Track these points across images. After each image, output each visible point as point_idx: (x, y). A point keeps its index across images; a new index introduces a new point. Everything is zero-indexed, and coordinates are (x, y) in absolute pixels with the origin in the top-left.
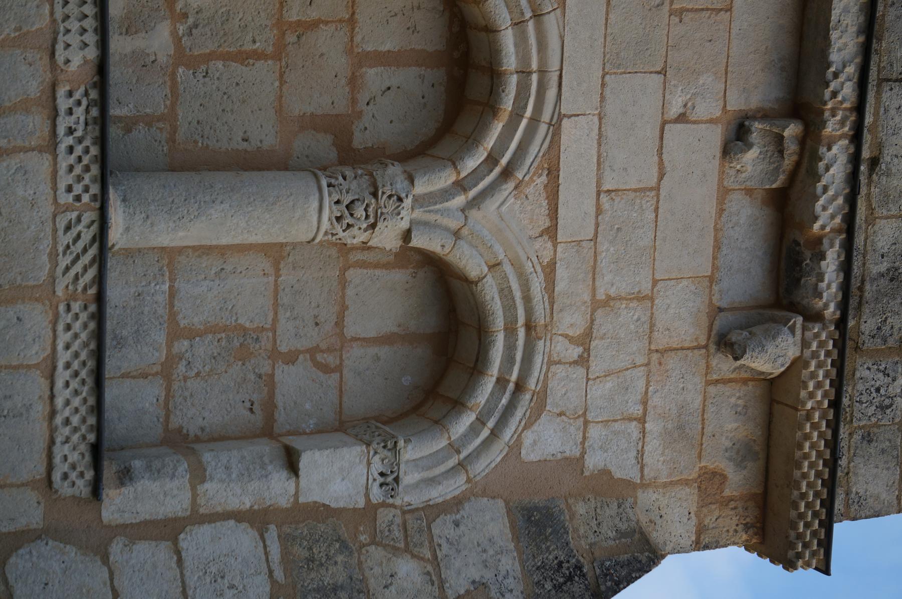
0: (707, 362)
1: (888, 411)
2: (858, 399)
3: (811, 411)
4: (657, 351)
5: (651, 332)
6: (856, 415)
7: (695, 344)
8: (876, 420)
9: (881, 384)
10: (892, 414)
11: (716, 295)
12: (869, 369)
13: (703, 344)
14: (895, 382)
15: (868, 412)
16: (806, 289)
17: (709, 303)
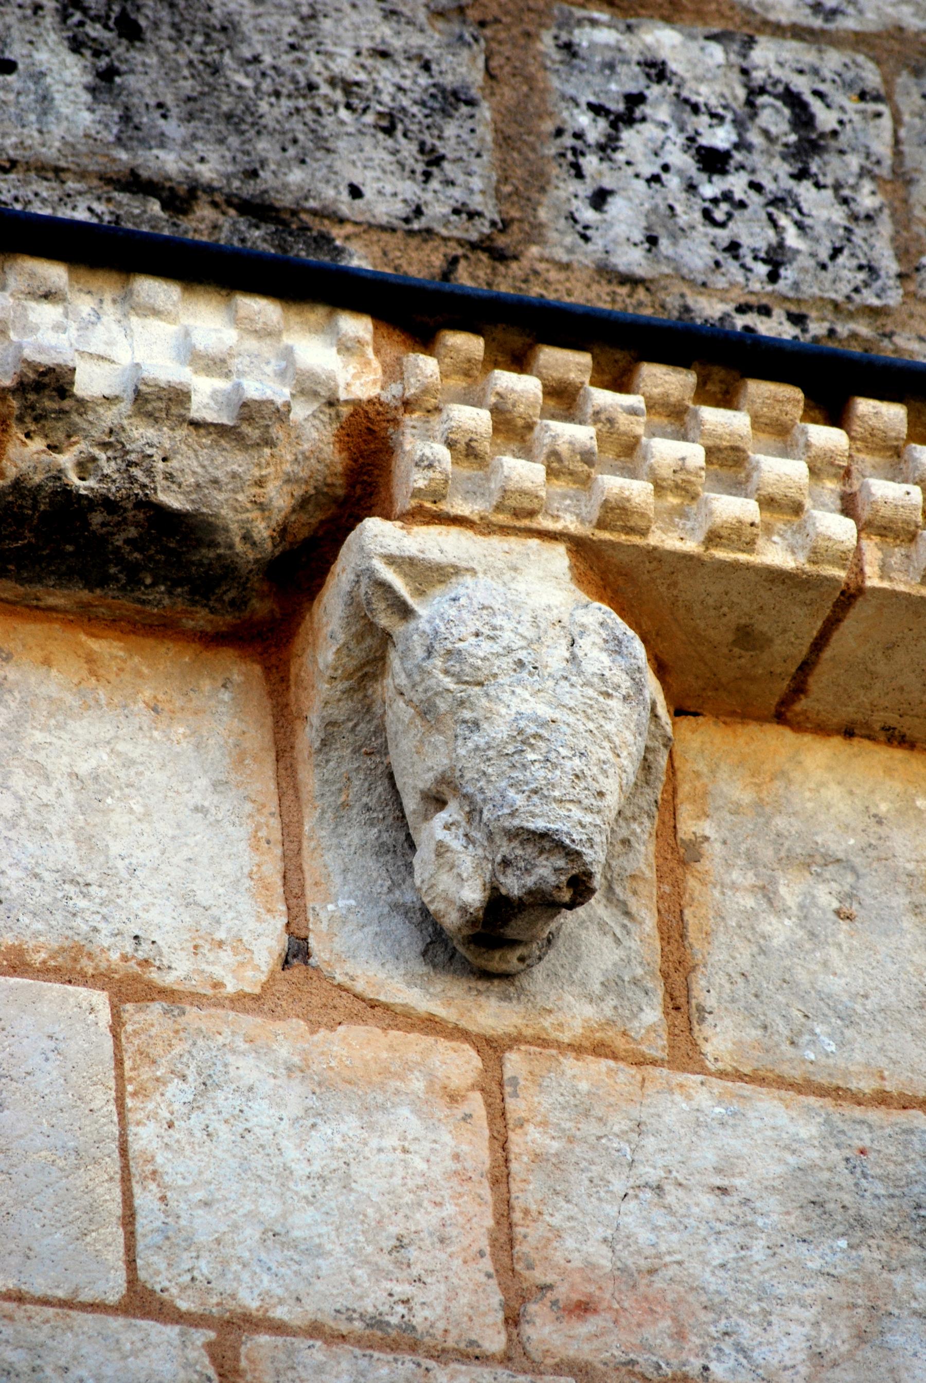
0: (577, 1049)
1: (825, 119)
2: (762, 269)
3: (865, 514)
4: (513, 1320)
5: (414, 1347)
6: (846, 289)
7: (476, 1104)
8: (867, 186)
9: (681, 140)
10: (839, 97)
11: (218, 972)
12: (600, 199)
13: (477, 1062)
14: (673, 66)
15: (829, 224)
16: (215, 481)
17: (260, 1011)
